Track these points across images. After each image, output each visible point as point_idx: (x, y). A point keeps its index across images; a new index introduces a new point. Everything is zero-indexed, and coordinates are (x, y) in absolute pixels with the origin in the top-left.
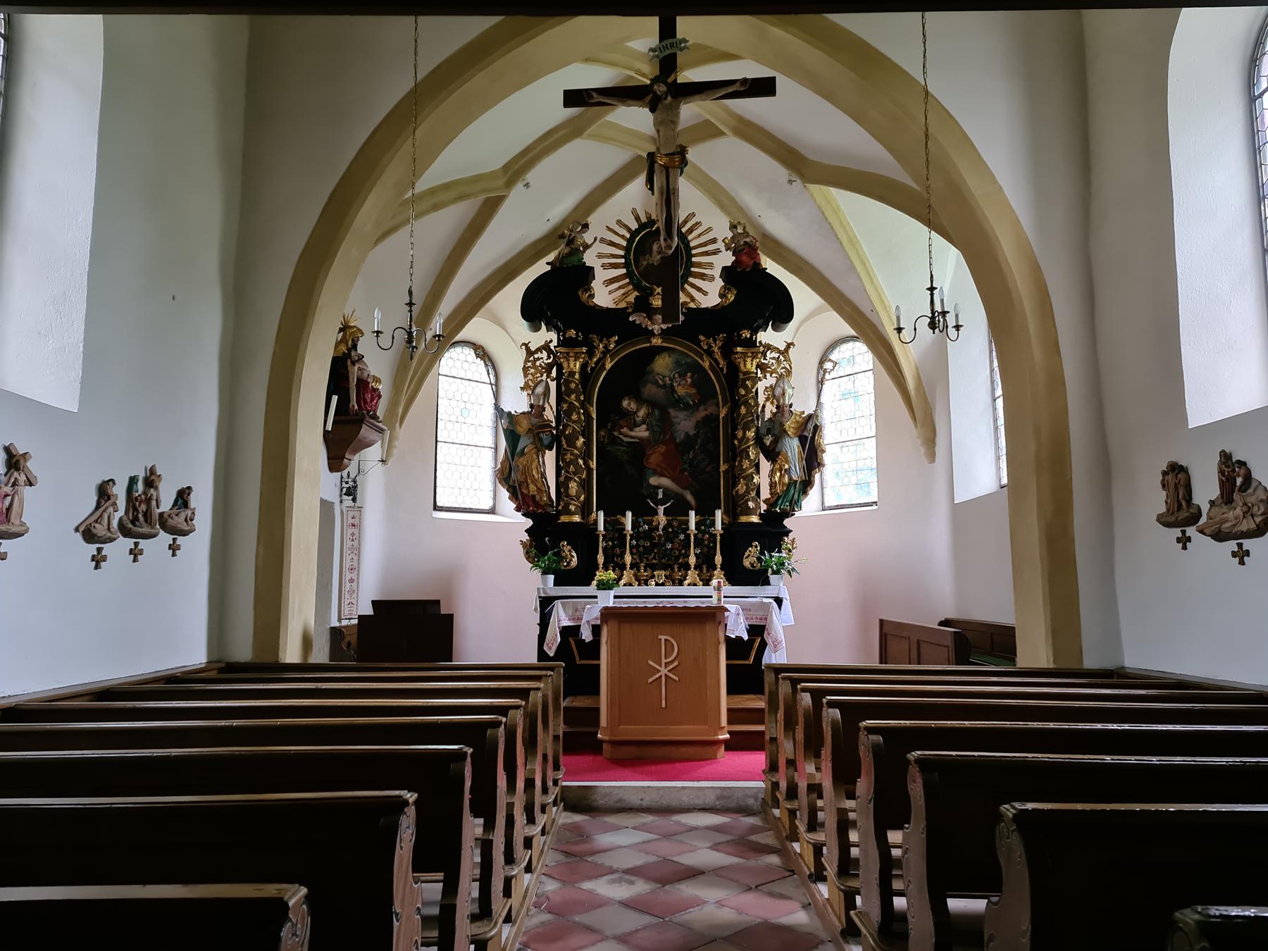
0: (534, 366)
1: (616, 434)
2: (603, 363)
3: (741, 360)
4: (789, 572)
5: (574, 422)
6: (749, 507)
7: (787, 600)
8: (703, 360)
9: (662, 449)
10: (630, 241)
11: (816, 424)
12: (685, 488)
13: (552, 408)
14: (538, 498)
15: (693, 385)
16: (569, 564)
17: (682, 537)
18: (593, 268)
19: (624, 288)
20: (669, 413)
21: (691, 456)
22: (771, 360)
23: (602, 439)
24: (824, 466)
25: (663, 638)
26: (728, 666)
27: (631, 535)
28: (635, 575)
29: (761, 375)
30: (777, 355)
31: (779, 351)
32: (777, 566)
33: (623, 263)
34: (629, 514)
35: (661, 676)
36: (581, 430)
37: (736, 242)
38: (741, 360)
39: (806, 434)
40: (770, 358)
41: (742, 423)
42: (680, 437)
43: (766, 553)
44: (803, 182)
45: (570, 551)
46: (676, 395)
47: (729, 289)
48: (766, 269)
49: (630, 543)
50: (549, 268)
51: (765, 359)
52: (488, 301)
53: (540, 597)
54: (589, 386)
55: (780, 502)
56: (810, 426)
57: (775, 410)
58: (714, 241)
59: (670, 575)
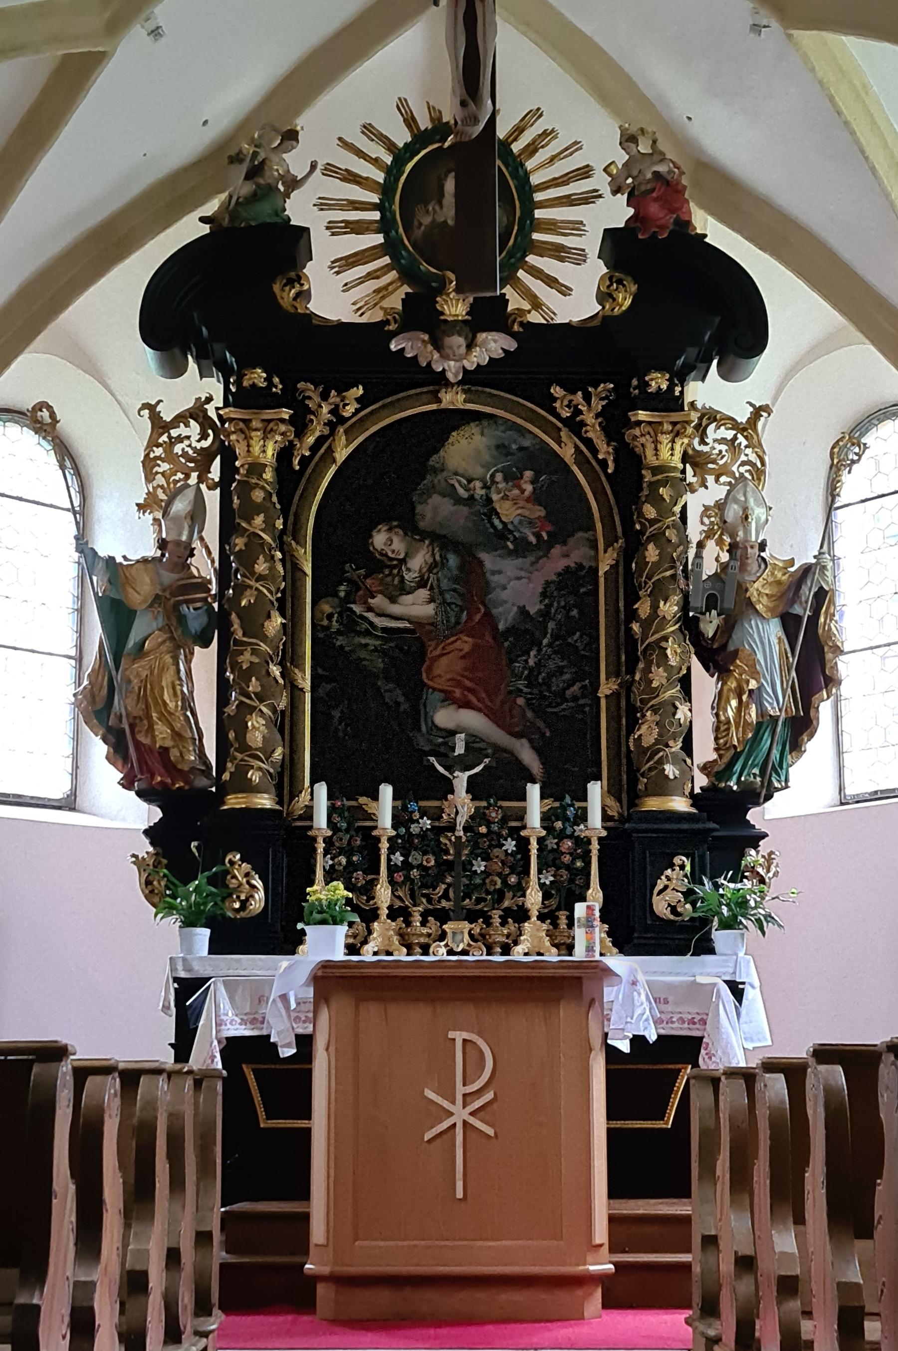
0: (170, 457)
1: (357, 609)
2: (330, 447)
3: (647, 440)
4: (759, 921)
5: (260, 578)
6: (667, 777)
7: (753, 987)
8: (559, 442)
9: (465, 643)
10: (393, 172)
11: (821, 588)
12: (518, 735)
13: (209, 553)
14: (174, 754)
15: (536, 498)
16: (244, 904)
17: (510, 845)
18: (307, 230)
19: (378, 278)
20: (481, 563)
21: (531, 662)
22: (716, 445)
23: (325, 623)
24: (839, 683)
25: (459, 1036)
26: (611, 1134)
27: (390, 839)
28: (401, 935)
29: (694, 480)
30: (730, 434)
31: (735, 425)
32: (730, 909)
33: (376, 222)
34: (387, 791)
35: (454, 1125)
36: (278, 599)
37: (635, 173)
38: (647, 440)
39: (797, 610)
40: (715, 441)
41: (650, 583)
42: (505, 619)
43: (706, 881)
44: (786, 28)
45: (247, 875)
46: (496, 522)
47: (620, 282)
48: (705, 236)
49: (389, 860)
50: (206, 229)
51: (703, 442)
52: (67, 306)
53: (175, 980)
54: (296, 498)
55: (738, 767)
56: (808, 592)
57: (725, 557)
58: (585, 172)
59: (483, 935)
